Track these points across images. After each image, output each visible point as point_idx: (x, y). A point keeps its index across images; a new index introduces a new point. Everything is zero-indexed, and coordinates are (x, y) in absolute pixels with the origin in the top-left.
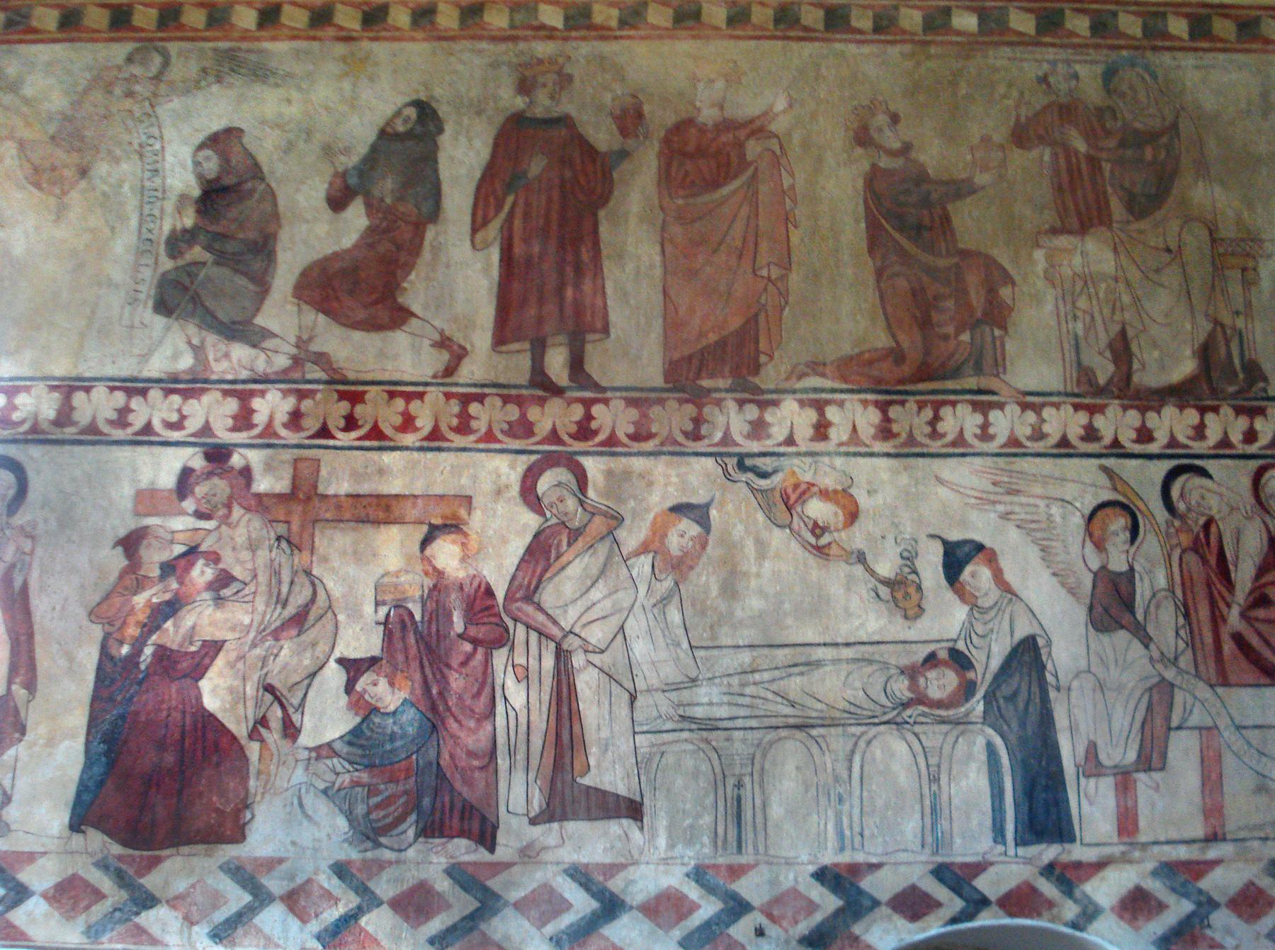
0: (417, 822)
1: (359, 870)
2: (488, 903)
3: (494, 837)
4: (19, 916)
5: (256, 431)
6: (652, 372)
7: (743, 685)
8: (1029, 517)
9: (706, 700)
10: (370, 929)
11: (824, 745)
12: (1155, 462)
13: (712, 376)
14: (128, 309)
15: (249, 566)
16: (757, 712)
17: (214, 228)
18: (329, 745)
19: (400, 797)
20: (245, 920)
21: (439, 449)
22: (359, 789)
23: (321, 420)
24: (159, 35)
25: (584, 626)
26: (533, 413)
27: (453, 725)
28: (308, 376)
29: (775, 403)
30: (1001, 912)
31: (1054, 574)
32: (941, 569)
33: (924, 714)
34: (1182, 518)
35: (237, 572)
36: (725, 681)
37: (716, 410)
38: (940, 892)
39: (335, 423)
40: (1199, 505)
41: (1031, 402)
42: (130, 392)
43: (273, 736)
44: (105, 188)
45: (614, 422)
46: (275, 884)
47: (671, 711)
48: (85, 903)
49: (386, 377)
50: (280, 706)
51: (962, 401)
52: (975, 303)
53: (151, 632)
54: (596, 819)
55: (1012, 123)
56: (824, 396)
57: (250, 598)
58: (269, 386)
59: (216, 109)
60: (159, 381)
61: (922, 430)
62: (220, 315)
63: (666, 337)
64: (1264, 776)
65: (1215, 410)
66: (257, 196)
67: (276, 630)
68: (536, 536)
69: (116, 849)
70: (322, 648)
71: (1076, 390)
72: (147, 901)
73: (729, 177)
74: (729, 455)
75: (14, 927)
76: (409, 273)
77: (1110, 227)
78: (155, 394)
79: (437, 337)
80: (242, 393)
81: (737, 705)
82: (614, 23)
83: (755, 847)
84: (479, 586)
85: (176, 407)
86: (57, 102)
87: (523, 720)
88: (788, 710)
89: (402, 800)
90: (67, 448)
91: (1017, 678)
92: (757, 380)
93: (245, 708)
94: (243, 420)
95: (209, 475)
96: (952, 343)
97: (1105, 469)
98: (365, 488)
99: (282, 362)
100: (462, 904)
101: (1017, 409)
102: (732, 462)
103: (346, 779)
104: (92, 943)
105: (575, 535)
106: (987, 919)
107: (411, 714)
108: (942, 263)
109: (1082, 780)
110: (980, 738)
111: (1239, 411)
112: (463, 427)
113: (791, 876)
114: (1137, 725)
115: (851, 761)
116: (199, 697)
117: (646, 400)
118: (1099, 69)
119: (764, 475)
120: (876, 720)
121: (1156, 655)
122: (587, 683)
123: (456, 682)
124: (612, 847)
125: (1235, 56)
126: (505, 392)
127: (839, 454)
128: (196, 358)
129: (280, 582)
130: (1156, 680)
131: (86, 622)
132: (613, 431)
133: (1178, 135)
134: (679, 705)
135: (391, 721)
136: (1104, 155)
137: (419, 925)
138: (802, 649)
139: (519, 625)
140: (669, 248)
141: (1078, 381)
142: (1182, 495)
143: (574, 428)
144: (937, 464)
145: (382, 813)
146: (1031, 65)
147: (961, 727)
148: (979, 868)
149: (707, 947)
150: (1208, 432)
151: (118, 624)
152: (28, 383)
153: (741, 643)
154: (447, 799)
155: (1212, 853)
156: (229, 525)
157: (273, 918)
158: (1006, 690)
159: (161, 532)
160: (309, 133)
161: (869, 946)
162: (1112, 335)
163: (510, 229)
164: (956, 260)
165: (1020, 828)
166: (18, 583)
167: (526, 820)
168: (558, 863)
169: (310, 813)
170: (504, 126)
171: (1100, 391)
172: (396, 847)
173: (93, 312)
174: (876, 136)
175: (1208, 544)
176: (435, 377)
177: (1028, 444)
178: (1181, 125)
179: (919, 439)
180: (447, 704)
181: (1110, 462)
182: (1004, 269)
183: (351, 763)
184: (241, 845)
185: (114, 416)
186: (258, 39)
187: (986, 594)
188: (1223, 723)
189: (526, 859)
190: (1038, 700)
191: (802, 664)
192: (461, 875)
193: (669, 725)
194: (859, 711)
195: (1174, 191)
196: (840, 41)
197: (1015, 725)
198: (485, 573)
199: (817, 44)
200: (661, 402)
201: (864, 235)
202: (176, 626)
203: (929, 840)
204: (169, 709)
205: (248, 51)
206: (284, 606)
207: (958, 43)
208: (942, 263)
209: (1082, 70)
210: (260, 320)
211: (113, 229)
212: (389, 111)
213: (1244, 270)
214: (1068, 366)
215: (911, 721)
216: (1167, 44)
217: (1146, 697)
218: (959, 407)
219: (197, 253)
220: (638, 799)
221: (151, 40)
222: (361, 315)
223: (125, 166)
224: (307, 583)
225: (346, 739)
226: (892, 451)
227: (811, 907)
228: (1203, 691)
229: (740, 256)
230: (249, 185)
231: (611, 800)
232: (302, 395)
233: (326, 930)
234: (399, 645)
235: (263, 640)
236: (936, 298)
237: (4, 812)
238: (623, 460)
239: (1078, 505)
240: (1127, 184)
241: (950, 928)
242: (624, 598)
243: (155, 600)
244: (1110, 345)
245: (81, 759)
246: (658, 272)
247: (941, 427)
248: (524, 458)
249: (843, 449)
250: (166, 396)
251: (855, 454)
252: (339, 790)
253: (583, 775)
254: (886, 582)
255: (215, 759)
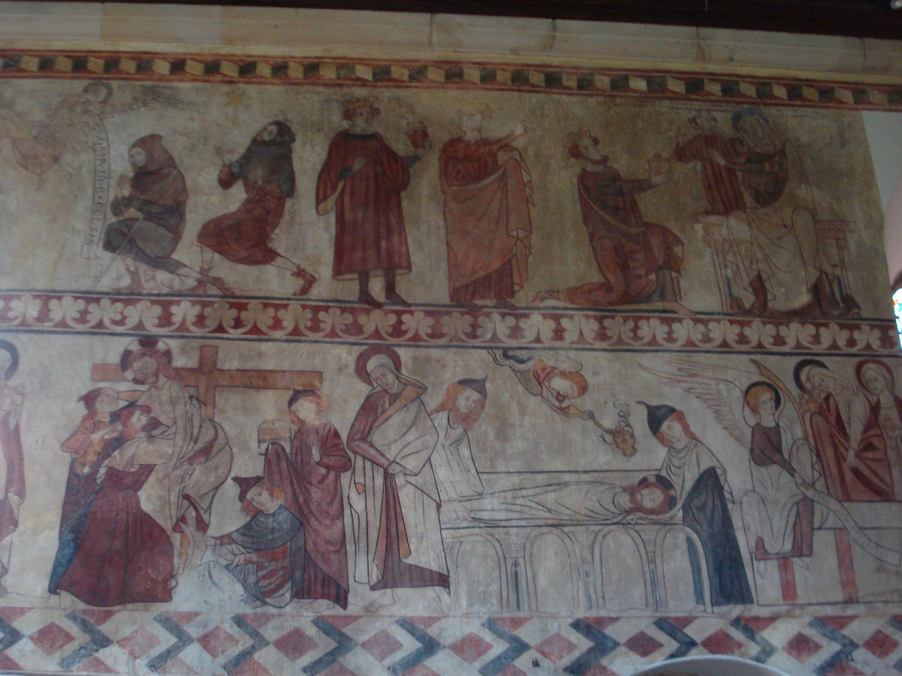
0: (292, 588)
1: (252, 621)
2: (343, 644)
3: (346, 598)
4: (13, 652)
5: (174, 327)
6: (441, 294)
7: (514, 498)
8: (704, 391)
9: (489, 507)
10: (261, 661)
11: (574, 539)
12: (788, 357)
13: (482, 298)
14: (86, 247)
15: (171, 415)
16: (525, 516)
17: (144, 197)
18: (229, 535)
19: (279, 571)
20: (172, 655)
21: (299, 341)
22: (251, 566)
23: (218, 321)
24: (105, 76)
25: (403, 457)
26: (362, 319)
27: (315, 523)
28: (209, 293)
29: (527, 316)
30: (705, 650)
31: (725, 428)
32: (646, 423)
33: (641, 518)
34: (810, 393)
35: (163, 419)
36: (502, 495)
37: (487, 319)
38: (661, 637)
39: (228, 322)
40: (820, 385)
41: (699, 317)
42: (88, 301)
43: (190, 529)
44: (70, 170)
45: (418, 326)
46: (193, 631)
47: (466, 514)
48: (58, 644)
49: (261, 294)
50: (194, 510)
51: (653, 317)
52: (657, 256)
53: (104, 458)
54: (417, 587)
55: (674, 146)
56: (559, 312)
57: (172, 436)
58: (183, 298)
59: (144, 123)
60: (107, 293)
61: (627, 334)
62: (148, 252)
63: (450, 272)
64: (881, 560)
65: (826, 325)
66: (171, 178)
67: (190, 458)
68: (368, 398)
69: (82, 606)
70: (223, 470)
71: (730, 312)
72: (104, 642)
73: (487, 174)
74: (497, 348)
75: (10, 660)
76: (275, 228)
77: (745, 211)
78: (105, 302)
79: (295, 270)
80: (165, 302)
81: (511, 511)
82: (406, 78)
83: (530, 606)
84: (330, 431)
85: (120, 310)
86: (38, 115)
87: (363, 520)
88: (547, 515)
89: (281, 573)
90: (46, 336)
91: (704, 495)
92: (513, 301)
93: (170, 510)
94: (165, 320)
95: (143, 355)
96: (644, 281)
97: (754, 362)
98: (249, 366)
99: (191, 283)
100: (325, 644)
101: (692, 323)
102: (499, 353)
103: (242, 558)
104: (65, 671)
105: (394, 398)
106: (695, 655)
107: (284, 515)
108: (633, 230)
109: (755, 562)
110: (681, 535)
111: (842, 327)
112: (315, 327)
113: (556, 626)
114: (790, 526)
115: (593, 549)
116: (138, 503)
117: (439, 312)
118: (730, 115)
119: (522, 362)
120: (609, 522)
121: (799, 481)
122: (407, 496)
123: (316, 494)
124: (429, 606)
125: (819, 110)
126: (343, 305)
127: (572, 349)
128: (132, 279)
129: (192, 426)
130: (801, 497)
131: (59, 451)
132: (417, 332)
133: (786, 156)
134: (471, 511)
135: (271, 519)
136: (737, 167)
137: (296, 658)
138: (553, 474)
139: (358, 456)
140: (449, 217)
141: (731, 307)
142: (808, 379)
143: (390, 329)
144: (639, 356)
145: (267, 582)
146: (684, 112)
147: (668, 527)
148: (688, 620)
149: (500, 674)
150: (822, 339)
151: (81, 453)
152: (19, 293)
153: (512, 470)
154: (312, 573)
155: (850, 611)
156: (157, 388)
157: (192, 653)
158: (697, 503)
159: (110, 392)
160: (206, 140)
161: (614, 674)
162: (752, 278)
163: (342, 203)
164: (642, 229)
165: (714, 594)
166: (12, 424)
167: (368, 587)
168: (391, 616)
169: (217, 581)
170: (335, 138)
171: (747, 312)
172: (278, 605)
173: (63, 249)
174: (584, 151)
175: (829, 410)
176: (294, 294)
177: (700, 345)
178: (787, 151)
179: (626, 340)
180: (310, 509)
181: (757, 357)
182: (675, 235)
183: (244, 548)
184: (169, 604)
185: (78, 316)
186: (170, 80)
187: (679, 440)
188: (850, 525)
189: (369, 614)
190: (720, 510)
191: (555, 484)
192: (325, 625)
193: (465, 524)
194: (596, 516)
195: (786, 190)
196: (556, 93)
197: (705, 526)
198: (333, 422)
199: (541, 95)
200: (448, 313)
201: (580, 212)
202: (121, 454)
203: (651, 601)
204: (117, 510)
205: (164, 88)
206: (196, 442)
207: (634, 97)
208: (633, 230)
209: (719, 116)
210: (175, 256)
211: (76, 196)
212: (258, 127)
213: (837, 239)
214: (723, 296)
215: (633, 522)
216: (773, 101)
217: (795, 508)
218: (651, 321)
219: (132, 212)
220: (445, 573)
221: (99, 79)
222: (244, 254)
223: (83, 157)
224: (211, 428)
225: (241, 531)
226: (608, 347)
227: (571, 647)
228: (834, 504)
229: (497, 224)
230: (166, 171)
231: (427, 573)
232: (205, 305)
233: (230, 662)
234: (276, 469)
235: (182, 464)
236: (630, 252)
237: (3, 580)
238: (425, 350)
239: (737, 384)
240: (754, 185)
241: (670, 661)
242: (430, 440)
243: (106, 437)
244: (751, 284)
245: (56, 544)
246: (443, 232)
247: (640, 333)
248: (357, 348)
249: (574, 346)
250: (113, 304)
251: (583, 349)
252: (237, 566)
253: (407, 556)
254: (609, 432)
255: (149, 545)
